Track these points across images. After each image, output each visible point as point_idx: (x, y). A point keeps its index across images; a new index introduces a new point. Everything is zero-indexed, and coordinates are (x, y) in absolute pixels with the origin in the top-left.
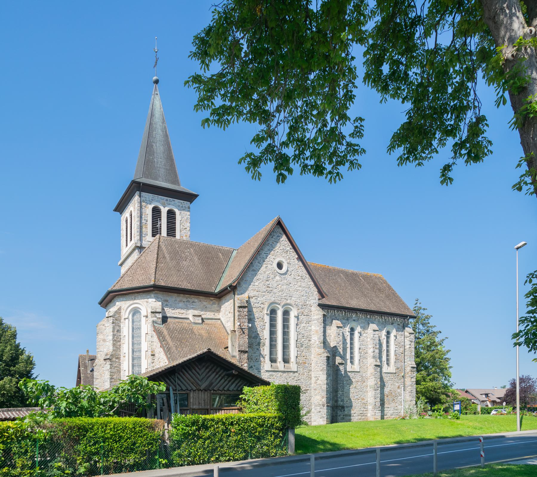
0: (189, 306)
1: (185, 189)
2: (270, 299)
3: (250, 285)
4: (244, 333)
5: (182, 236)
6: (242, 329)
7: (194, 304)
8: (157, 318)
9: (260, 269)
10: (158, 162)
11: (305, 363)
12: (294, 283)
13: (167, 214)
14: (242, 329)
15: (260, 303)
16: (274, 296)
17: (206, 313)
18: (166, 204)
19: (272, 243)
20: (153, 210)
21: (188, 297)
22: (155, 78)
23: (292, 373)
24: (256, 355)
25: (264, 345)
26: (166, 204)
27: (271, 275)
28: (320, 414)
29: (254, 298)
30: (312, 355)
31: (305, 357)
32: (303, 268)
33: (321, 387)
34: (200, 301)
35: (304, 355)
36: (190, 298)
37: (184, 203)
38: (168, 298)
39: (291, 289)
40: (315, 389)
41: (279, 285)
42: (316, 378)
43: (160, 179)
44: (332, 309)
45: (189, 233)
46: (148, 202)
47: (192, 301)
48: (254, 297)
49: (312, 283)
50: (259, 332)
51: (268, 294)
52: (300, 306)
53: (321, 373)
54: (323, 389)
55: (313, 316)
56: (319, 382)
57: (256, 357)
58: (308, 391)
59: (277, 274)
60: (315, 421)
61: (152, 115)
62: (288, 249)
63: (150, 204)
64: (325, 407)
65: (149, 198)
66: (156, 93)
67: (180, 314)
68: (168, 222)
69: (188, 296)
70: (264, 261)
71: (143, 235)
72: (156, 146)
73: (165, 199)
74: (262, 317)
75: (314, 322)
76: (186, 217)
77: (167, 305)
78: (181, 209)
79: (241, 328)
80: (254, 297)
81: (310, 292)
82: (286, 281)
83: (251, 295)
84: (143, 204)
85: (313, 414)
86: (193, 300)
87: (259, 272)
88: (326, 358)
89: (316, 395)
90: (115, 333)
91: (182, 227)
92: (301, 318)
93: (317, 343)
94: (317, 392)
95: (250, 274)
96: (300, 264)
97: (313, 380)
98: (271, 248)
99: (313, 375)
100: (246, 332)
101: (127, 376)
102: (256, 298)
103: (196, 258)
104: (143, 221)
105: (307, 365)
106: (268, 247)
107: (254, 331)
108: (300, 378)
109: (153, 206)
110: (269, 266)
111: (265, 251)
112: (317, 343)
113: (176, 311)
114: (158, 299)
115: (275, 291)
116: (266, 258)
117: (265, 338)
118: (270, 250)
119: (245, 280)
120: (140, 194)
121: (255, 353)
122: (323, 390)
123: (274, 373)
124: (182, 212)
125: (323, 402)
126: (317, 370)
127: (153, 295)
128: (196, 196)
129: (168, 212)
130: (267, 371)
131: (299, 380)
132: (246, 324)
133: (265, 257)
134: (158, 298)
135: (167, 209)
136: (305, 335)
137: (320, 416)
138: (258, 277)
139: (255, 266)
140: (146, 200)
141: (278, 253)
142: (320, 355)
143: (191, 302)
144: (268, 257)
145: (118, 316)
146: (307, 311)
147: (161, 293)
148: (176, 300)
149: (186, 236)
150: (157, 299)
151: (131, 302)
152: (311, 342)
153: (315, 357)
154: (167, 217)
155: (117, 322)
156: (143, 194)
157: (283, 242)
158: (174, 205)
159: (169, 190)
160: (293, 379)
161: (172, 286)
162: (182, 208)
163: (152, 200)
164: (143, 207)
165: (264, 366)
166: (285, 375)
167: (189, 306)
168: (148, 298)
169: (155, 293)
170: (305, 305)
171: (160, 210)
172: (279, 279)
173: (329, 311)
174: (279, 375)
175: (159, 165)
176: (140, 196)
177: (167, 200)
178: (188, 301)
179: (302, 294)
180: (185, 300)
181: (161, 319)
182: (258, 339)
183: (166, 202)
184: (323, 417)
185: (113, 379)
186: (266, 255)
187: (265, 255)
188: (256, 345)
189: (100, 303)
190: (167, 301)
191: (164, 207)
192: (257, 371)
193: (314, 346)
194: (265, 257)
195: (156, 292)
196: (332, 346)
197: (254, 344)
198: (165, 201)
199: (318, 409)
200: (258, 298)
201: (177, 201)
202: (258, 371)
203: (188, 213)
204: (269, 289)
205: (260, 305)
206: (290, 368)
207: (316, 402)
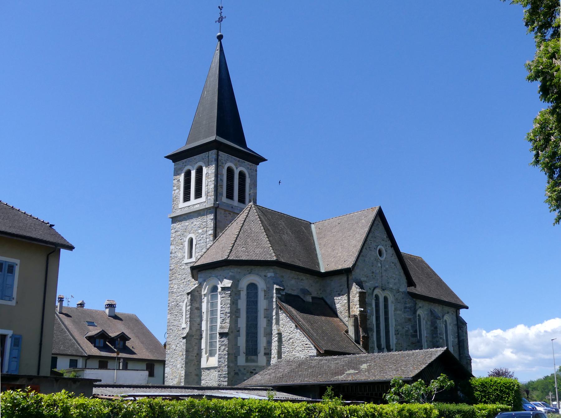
37: (252, 165)
93: (411, 331)
120: (218, 153)
127: (272, 270)
128: (264, 160)
177: (239, 161)
178: (298, 279)
189: (193, 269)
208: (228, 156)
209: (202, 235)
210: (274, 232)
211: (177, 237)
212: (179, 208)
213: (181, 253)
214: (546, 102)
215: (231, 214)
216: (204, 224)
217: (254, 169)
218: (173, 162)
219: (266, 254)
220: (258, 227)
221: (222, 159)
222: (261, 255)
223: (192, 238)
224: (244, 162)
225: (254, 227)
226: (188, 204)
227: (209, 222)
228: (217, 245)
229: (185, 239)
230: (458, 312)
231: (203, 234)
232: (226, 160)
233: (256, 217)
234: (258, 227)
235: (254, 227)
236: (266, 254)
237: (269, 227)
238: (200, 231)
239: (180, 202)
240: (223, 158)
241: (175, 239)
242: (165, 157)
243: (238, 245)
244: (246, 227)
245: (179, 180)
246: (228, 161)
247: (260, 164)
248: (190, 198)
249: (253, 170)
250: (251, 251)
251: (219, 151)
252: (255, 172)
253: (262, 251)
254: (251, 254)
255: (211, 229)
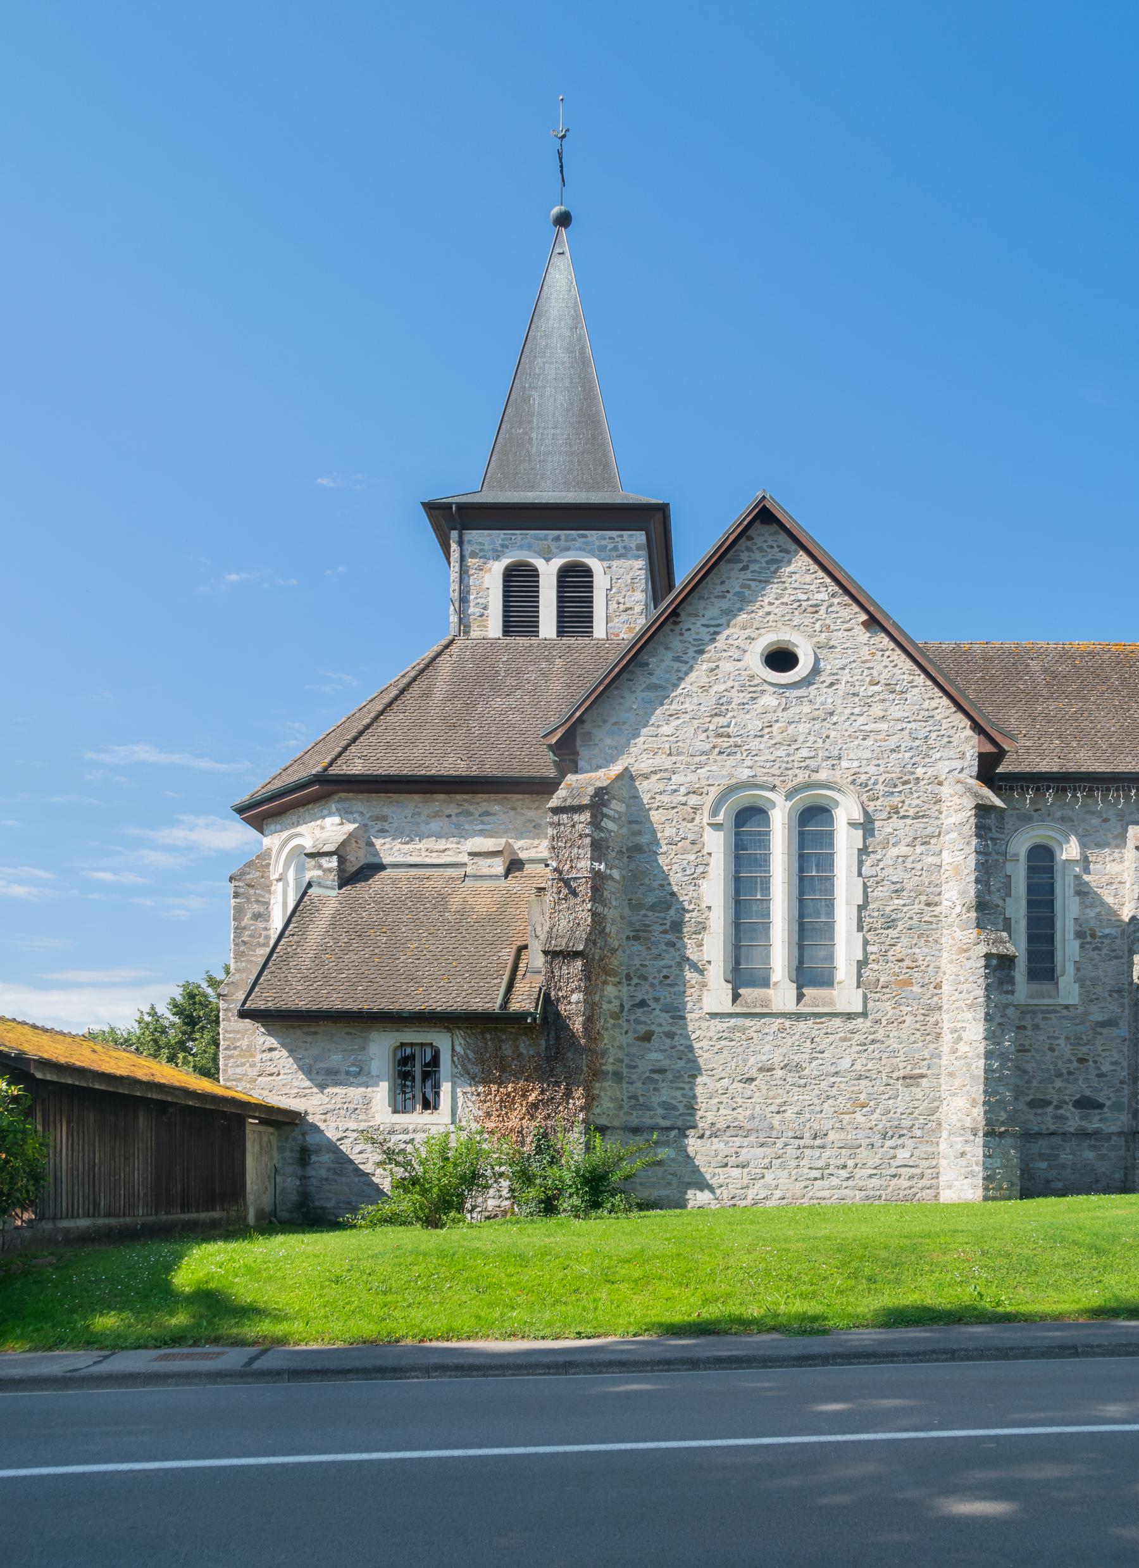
0: (467, 827)
1: (631, 495)
2: (731, 776)
3: (636, 735)
4: (575, 894)
6: (566, 883)
7: (486, 819)
8: (324, 871)
9: (681, 679)
11: (909, 983)
12: (848, 711)
14: (566, 883)
15: (683, 790)
16: (748, 763)
17: (536, 842)
18: (555, 551)
19: (742, 586)
21: (465, 800)
22: (556, 210)
23: (837, 1022)
24: (662, 963)
25: (702, 928)
26: (555, 551)
27: (734, 693)
28: (962, 1162)
29: (654, 778)
30: (945, 955)
31: (907, 963)
32: (898, 656)
33: (969, 1065)
34: (514, 809)
35: (899, 956)
36: (472, 803)
37: (622, 536)
38: (386, 811)
39: (833, 734)
40: (951, 1075)
41: (776, 726)
42: (955, 1035)
44: (1113, 787)
46: (490, 554)
47: (481, 810)
48: (655, 772)
49: (945, 701)
50: (675, 889)
51: (724, 756)
52: (880, 787)
53: (969, 1015)
54: (976, 1072)
55: (947, 817)
56: (963, 1048)
57: (665, 972)
58: (924, 1081)
59: (766, 687)
60: (950, 1187)
62: (823, 596)
63: (497, 558)
64: (980, 1140)
65: (493, 543)
67: (434, 854)
68: (561, 600)
69: (465, 796)
70: (702, 652)
73: (551, 537)
74: (691, 837)
75: (947, 837)
77: (382, 831)
78: (603, 554)
79: (562, 880)
80: (655, 772)
81: (934, 735)
82: (807, 709)
83: (643, 765)
85: (943, 1163)
86: (485, 806)
87: (679, 691)
88: (982, 962)
89: (954, 1094)
90: (246, 921)
91: (613, 606)
92: (884, 828)
94: (957, 1082)
95: (632, 699)
96: (884, 641)
97: (947, 1038)
98: (738, 605)
99: (946, 1025)
100: (584, 889)
101: (1101, 1034)
102: (666, 775)
105: (916, 989)
106: (724, 604)
107: (655, 884)
108: (879, 1036)
109: (506, 562)
110: (727, 666)
111: (707, 617)
112: (958, 909)
113: (418, 847)
114: (351, 817)
115: (754, 744)
116: (713, 640)
117: (703, 906)
118: (730, 614)
119: (616, 723)
121: (659, 957)
122: (973, 1077)
123: (748, 1022)
124: (615, 563)
125: (974, 1120)
126: (957, 1004)
130: (714, 1015)
131: (873, 1042)
132: (585, 864)
133: (707, 638)
134: (351, 813)
135: (557, 563)
136: (909, 885)
137: (963, 1171)
138: (674, 706)
139: (659, 672)
141: (771, 618)
142: (966, 951)
143: (477, 814)
144: (721, 638)
145: (258, 874)
146: (915, 802)
147: (361, 796)
148: (419, 814)
150: (346, 814)
151: (286, 834)
152: (938, 909)
153: (951, 962)
155: (252, 891)
156: (472, 535)
157: (795, 577)
158: (584, 550)
159: (521, 509)
160: (844, 1039)
161: (392, 772)
162: (614, 554)
164: (472, 572)
165: (700, 1000)
166: (802, 1026)
167: (467, 827)
168: (324, 817)
169: (341, 800)
170: (905, 783)
171: (536, 570)
172: (776, 703)
173: (1098, 795)
174: (775, 1027)
177: (558, 539)
178: (468, 814)
179: (892, 743)
180: (452, 809)
181: (335, 873)
182: (672, 912)
183: (553, 545)
184: (972, 1174)
185: (235, 1048)
186: (712, 630)
187: (705, 629)
188: (665, 932)
190: (384, 818)
191: (548, 560)
192: (667, 1016)
193: (950, 920)
194: (707, 638)
195: (342, 795)
196: (1127, 920)
197: (656, 927)
199: (959, 1147)
200: (673, 777)
201: (593, 535)
202: (672, 1017)
204: (724, 743)
205: (684, 799)
206: (832, 1003)
207: (955, 1117)
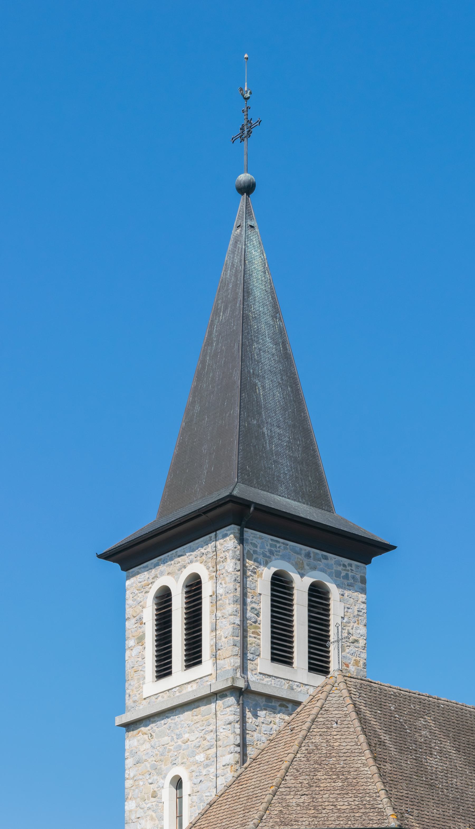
5: (347, 661)
10: (272, 437)
13: (310, 595)
18: (307, 567)
20: (273, 584)
22: (244, 177)
26: (307, 567)
37: (350, 565)
43: (282, 488)
45: (364, 655)
46: (261, 558)
61: (247, 292)
63: (266, 564)
66: (249, 223)
71: (250, 656)
72: (263, 387)
73: (303, 552)
76: (356, 608)
84: (250, 563)
103: (448, 745)
104: (249, 614)
109: (273, 570)
120: (242, 533)
124: (347, 593)
129: (310, 589)
135: (308, 581)
140: (255, 552)
149: (357, 663)
154: (309, 606)
156: (249, 533)
162: (346, 582)
163: (271, 552)
164: (249, 573)
175: (276, 446)
176: (241, 540)
177: (308, 555)
183: (306, 561)
191: (302, 576)
198: (302, 557)
201: (333, 559)
203: (362, 597)
208: (272, 540)
209: (204, 768)
210: (401, 751)
211: (141, 777)
212: (144, 697)
213: (152, 819)
214: (246, 96)
215: (287, 707)
216: (208, 737)
217: (358, 577)
218: (123, 569)
219: (367, 811)
220: (352, 737)
221: (254, 551)
222: (352, 814)
223: (181, 778)
224: (326, 558)
225: (338, 737)
226: (166, 683)
227: (222, 730)
228: (235, 792)
229: (162, 781)
230: (211, 698)
231: (207, 766)
232: (268, 554)
233: (345, 709)
234: (352, 737)
235: (338, 737)
236: (367, 811)
237: (385, 737)
238: (200, 757)
239: (146, 680)
240: (258, 549)
241: (137, 783)
242: (100, 556)
243: (288, 789)
244: (317, 739)
245: (141, 619)
246: (273, 558)
247: (373, 559)
248: (171, 668)
249: (353, 578)
250: (326, 803)
251: (245, 529)
252: (360, 584)
253: (357, 803)
254: (324, 811)
255: (228, 749)
